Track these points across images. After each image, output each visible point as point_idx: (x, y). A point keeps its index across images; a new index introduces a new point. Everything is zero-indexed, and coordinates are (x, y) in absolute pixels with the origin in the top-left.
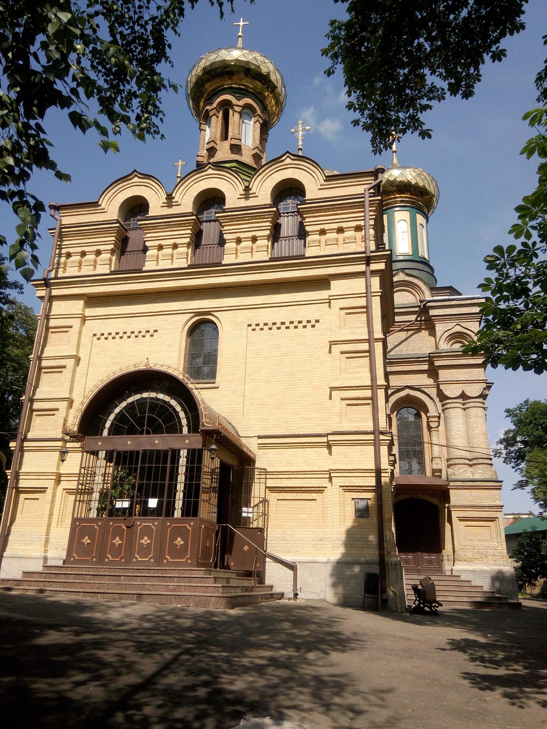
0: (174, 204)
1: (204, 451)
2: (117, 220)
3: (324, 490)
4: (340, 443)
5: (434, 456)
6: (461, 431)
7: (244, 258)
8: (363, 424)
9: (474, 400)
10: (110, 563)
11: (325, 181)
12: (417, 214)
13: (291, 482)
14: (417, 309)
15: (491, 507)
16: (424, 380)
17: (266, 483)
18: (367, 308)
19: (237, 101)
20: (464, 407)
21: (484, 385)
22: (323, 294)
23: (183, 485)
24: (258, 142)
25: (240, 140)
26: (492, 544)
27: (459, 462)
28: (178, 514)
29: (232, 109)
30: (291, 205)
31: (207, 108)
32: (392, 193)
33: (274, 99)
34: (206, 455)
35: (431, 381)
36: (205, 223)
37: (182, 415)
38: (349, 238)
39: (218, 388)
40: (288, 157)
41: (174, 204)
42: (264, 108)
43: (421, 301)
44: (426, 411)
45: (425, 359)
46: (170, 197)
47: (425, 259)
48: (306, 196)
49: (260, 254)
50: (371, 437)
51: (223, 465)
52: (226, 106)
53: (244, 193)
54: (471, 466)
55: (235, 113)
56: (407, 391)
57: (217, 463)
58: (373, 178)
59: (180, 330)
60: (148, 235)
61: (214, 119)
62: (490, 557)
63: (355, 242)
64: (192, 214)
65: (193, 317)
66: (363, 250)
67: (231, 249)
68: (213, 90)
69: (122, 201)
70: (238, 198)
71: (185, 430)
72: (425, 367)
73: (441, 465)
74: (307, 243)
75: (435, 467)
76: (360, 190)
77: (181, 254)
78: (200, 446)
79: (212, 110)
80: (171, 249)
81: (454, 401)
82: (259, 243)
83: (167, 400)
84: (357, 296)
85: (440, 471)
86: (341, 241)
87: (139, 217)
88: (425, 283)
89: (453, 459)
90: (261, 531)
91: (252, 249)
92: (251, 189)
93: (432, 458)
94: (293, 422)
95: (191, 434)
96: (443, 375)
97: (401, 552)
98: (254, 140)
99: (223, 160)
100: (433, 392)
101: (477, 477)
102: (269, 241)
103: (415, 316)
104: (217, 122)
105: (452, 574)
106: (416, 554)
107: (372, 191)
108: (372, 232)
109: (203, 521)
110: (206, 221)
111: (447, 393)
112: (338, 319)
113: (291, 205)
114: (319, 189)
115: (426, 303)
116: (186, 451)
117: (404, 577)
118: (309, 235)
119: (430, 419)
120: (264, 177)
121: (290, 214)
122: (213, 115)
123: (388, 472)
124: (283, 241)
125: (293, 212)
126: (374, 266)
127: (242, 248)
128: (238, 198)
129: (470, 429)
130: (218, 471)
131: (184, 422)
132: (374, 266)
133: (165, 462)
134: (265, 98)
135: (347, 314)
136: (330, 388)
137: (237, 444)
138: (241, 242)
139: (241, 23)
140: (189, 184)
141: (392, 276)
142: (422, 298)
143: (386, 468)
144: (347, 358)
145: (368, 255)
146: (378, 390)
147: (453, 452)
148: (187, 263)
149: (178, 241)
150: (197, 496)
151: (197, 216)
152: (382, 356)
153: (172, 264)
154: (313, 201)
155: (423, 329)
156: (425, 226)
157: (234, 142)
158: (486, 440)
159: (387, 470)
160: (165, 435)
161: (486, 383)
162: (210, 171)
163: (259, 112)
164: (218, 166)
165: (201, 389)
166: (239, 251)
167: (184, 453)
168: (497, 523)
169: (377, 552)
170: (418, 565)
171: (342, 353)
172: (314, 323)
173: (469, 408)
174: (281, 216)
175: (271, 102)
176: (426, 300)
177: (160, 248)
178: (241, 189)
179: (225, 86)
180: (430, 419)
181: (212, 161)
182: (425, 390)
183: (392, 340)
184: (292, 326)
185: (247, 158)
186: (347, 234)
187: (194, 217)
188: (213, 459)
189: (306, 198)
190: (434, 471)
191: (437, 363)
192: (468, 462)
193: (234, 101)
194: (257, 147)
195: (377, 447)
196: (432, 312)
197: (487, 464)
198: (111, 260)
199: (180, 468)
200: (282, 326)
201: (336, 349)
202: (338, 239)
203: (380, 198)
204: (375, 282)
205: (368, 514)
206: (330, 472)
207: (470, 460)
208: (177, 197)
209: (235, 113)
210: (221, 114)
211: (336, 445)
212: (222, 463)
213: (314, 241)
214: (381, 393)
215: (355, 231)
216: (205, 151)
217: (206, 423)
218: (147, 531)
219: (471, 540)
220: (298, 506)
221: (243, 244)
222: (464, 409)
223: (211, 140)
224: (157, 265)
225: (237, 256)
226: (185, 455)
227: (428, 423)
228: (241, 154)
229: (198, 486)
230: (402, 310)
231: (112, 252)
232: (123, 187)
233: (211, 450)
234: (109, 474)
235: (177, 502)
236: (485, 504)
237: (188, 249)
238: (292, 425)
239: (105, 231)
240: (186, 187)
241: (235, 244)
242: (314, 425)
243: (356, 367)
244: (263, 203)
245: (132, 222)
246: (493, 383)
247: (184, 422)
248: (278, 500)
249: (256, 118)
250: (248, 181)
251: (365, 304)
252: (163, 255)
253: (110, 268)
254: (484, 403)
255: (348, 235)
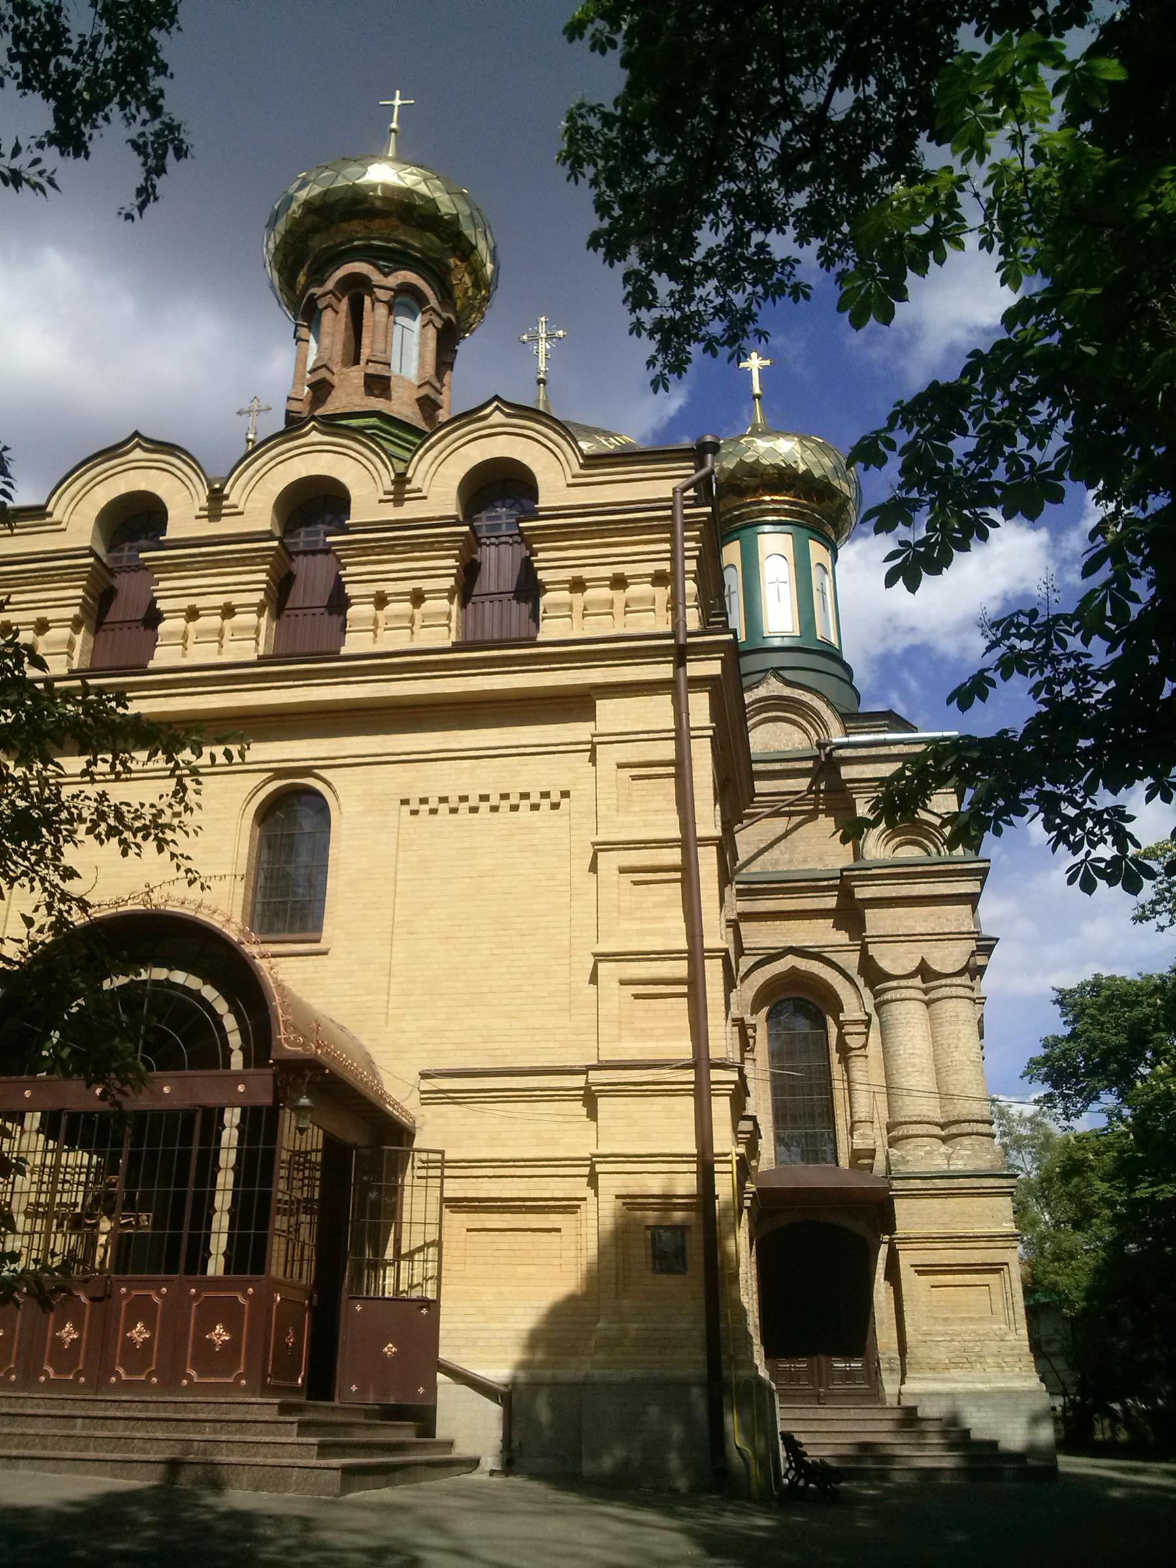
0: (224, 511)
1: (281, 1111)
2: (89, 548)
3: (579, 1207)
4: (616, 1090)
5: (856, 1119)
6: (920, 1056)
7: (393, 640)
8: (672, 1044)
9: (948, 981)
10: (193, 1387)
11: (582, 466)
12: (810, 541)
13: (500, 1186)
14: (810, 764)
15: (991, 1238)
16: (823, 933)
17: (442, 1187)
18: (681, 769)
19: (381, 277)
20: (927, 998)
21: (972, 945)
22: (580, 731)
23: (229, 1196)
24: (430, 370)
25: (389, 365)
26: (995, 1327)
27: (915, 1132)
28: (215, 1267)
29: (371, 294)
30: (504, 520)
31: (312, 291)
32: (754, 491)
33: (470, 274)
34: (288, 1121)
35: (842, 937)
36: (301, 557)
37: (230, 1022)
38: (639, 600)
39: (325, 953)
40: (497, 408)
41: (224, 511)
42: (446, 294)
43: (821, 746)
44: (836, 1006)
45: (831, 882)
46: (216, 497)
47: (830, 645)
48: (540, 500)
49: (431, 633)
50: (690, 1075)
51: (330, 1144)
52: (357, 288)
53: (392, 488)
54: (944, 1140)
55: (377, 304)
56: (790, 961)
57: (314, 1138)
58: (692, 464)
59: (236, 810)
60: (162, 585)
61: (328, 317)
62: (990, 1360)
63: (653, 610)
64: (268, 536)
65: (270, 780)
66: (668, 629)
67: (363, 620)
68: (330, 248)
69: (102, 503)
70: (381, 501)
71: (237, 1061)
72: (831, 902)
73: (872, 1137)
74: (542, 608)
75: (859, 1143)
76: (664, 489)
77: (243, 629)
78: (268, 1100)
79: (324, 295)
80: (218, 618)
81: (903, 983)
82: (429, 605)
83: (194, 987)
84: (653, 736)
85: (871, 1154)
86: (619, 607)
87: (143, 543)
88: (829, 704)
89: (906, 1123)
90: (428, 1307)
91: (412, 619)
92: (409, 481)
93: (853, 1124)
94: (506, 1038)
95: (252, 1070)
96: (877, 921)
97: (793, 1354)
98: (422, 366)
99: (347, 410)
100: (851, 961)
101: (958, 1165)
102: (451, 602)
103: (808, 780)
104: (334, 322)
105: (899, 1403)
106: (815, 1359)
107: (691, 493)
108: (691, 587)
109: (277, 1285)
110: (305, 553)
111: (886, 964)
112: (614, 789)
113: (504, 520)
114: (569, 485)
115: (831, 750)
116: (238, 1111)
117: (779, 1414)
118: (546, 591)
119: (847, 1029)
120: (441, 453)
121: (503, 539)
122: (326, 308)
123: (730, 1162)
124: (487, 604)
125: (511, 536)
126: (696, 669)
127: (388, 617)
128: (381, 501)
129: (940, 1052)
130: (319, 1159)
131: (235, 1040)
132: (696, 669)
133: (187, 1138)
134: (449, 270)
135: (634, 778)
136: (595, 955)
137: (370, 1095)
138: (387, 603)
139: (397, 102)
140: (264, 465)
141: (741, 691)
142: (824, 737)
143: (726, 1150)
144: (635, 883)
145: (682, 642)
146: (707, 962)
147: (901, 1108)
148: (256, 650)
149: (236, 599)
150: (264, 1222)
151: (280, 539)
152: (717, 879)
153: (220, 653)
154: (557, 512)
155: (822, 811)
156: (829, 569)
157: (373, 369)
158: (978, 1077)
159: (727, 1155)
160: (186, 1072)
161: (977, 940)
162: (315, 436)
163: (433, 302)
164: (331, 424)
165: (274, 956)
166: (381, 624)
167: (232, 1117)
168: (1007, 1276)
169: (702, 1357)
170: (820, 1386)
171: (623, 870)
172: (557, 799)
173: (938, 999)
174: (480, 545)
175: (462, 280)
176: (831, 743)
177: (193, 614)
178: (387, 480)
179: (356, 243)
180: (847, 1029)
181: (318, 413)
182: (834, 957)
183: (747, 840)
184: (505, 804)
185: (402, 405)
186: (633, 590)
187: (275, 544)
188: (302, 1131)
189: (540, 505)
190: (856, 1155)
191: (861, 893)
192: (937, 1131)
193: (376, 277)
194: (428, 383)
195: (705, 1100)
196: (847, 772)
197: (982, 1135)
198: (71, 644)
199: (223, 1155)
200: (482, 804)
201: (609, 862)
202: (612, 601)
203: (709, 509)
204: (700, 706)
205: (684, 1262)
206: (592, 1161)
207: (943, 1126)
208: (235, 494)
209: (377, 304)
210: (344, 305)
211: (606, 1094)
212: (329, 1140)
213: (557, 605)
214: (713, 970)
215: (653, 584)
216: (307, 389)
217: (287, 1042)
218: (142, 1310)
219: (946, 1319)
220: (517, 1246)
221: (392, 608)
222: (928, 1004)
223: (320, 364)
224: (184, 656)
225: (376, 636)
226: (237, 1121)
227: (841, 1037)
228: (389, 398)
229: (266, 1198)
230: (777, 766)
231: (76, 624)
232: (106, 471)
233: (297, 1109)
234: (67, 1166)
235: (213, 1238)
236: (978, 1231)
237: (259, 617)
238: (504, 1045)
239: (62, 576)
240: (258, 471)
241: (372, 607)
242: (557, 1044)
243: (656, 906)
244: (438, 514)
245: (126, 553)
246: (997, 940)
247: (235, 1040)
248: (468, 1230)
249: (427, 316)
250: (405, 461)
251: (671, 755)
252: (199, 633)
253: (69, 663)
254: (972, 989)
255: (637, 594)
